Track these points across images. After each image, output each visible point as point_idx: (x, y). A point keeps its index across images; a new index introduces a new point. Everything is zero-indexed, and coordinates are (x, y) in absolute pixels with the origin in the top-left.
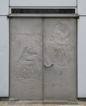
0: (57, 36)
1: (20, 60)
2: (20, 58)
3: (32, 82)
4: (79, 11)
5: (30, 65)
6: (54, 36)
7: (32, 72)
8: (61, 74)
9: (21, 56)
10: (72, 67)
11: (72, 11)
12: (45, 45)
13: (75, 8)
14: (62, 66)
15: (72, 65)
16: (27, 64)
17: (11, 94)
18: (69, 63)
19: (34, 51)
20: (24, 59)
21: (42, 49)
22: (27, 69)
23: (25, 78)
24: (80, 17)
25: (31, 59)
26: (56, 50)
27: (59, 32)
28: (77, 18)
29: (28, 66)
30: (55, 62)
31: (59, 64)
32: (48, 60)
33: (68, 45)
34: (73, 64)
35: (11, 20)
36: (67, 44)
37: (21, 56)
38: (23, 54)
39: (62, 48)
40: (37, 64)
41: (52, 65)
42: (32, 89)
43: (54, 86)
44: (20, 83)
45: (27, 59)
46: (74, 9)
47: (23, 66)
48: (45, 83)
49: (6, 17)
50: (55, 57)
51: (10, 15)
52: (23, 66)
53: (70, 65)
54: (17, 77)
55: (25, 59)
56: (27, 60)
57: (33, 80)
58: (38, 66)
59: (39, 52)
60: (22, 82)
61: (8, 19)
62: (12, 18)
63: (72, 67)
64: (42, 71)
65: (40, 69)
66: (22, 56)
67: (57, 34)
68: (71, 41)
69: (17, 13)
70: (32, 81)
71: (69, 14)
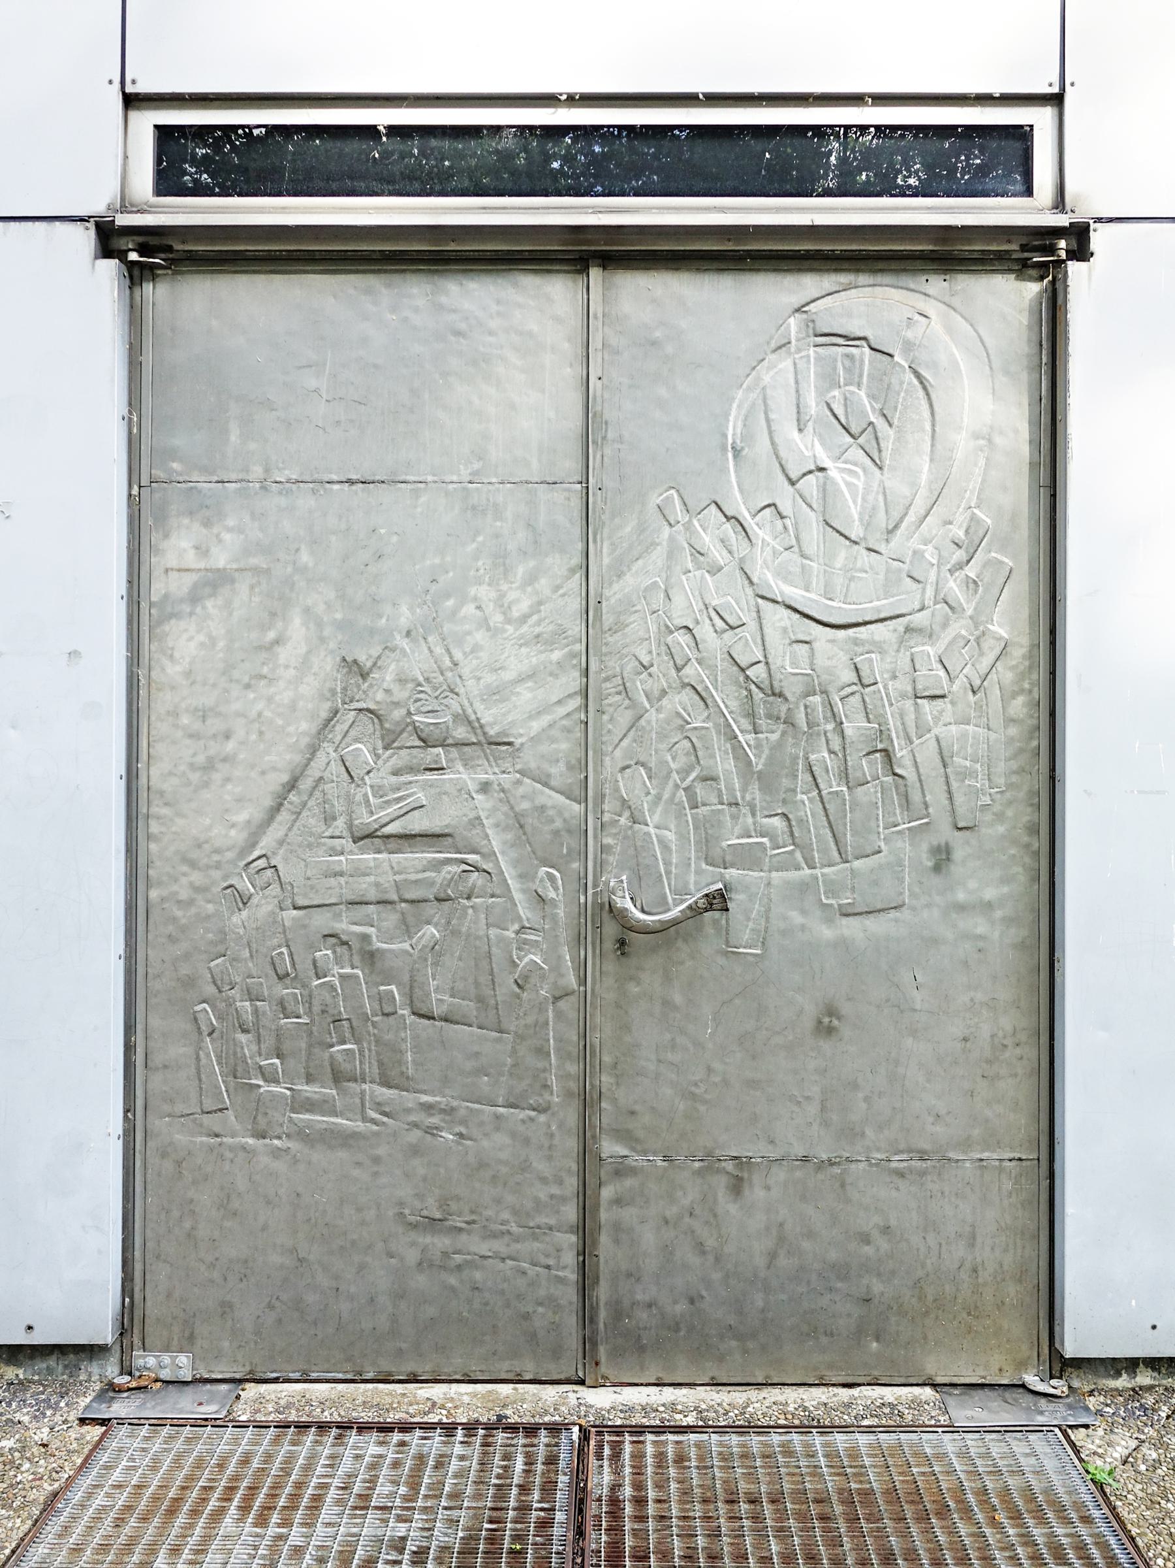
0: (786, 507)
1: (266, 843)
2: (277, 808)
3: (431, 1131)
4: (1090, 166)
5: (409, 906)
6: (738, 505)
7: (439, 1000)
8: (827, 1025)
9: (292, 785)
10: (980, 926)
11: (1000, 154)
12: (618, 627)
13: (1040, 119)
14: (846, 913)
15: (988, 907)
16: (365, 887)
17: (154, 1307)
18: (937, 869)
19: (462, 718)
20: (329, 819)
21: (572, 680)
22: (371, 957)
23: (338, 1077)
24: (1099, 239)
25: (417, 823)
26: (765, 696)
27: (807, 447)
28: (1048, 253)
29: (390, 919)
30: (748, 858)
31: (805, 887)
32: (660, 829)
33: (929, 635)
34: (990, 894)
35: (154, 292)
36: (920, 619)
37: (285, 778)
38: (313, 750)
39: (848, 676)
40: (507, 892)
41: (718, 901)
42: (432, 1224)
43: (737, 1187)
44: (276, 1153)
45: (365, 819)
46: (1022, 135)
47: (321, 921)
48: (610, 1148)
49: (85, 239)
50: (755, 793)
51: (125, 206)
52: (321, 921)
53: (961, 908)
54: (235, 1069)
55: (340, 824)
56: (366, 837)
57: (450, 1111)
58: (525, 912)
59: (536, 726)
60: (302, 1134)
61: (110, 267)
62: (154, 241)
63: (980, 926)
64: (572, 981)
65: (550, 959)
66: (305, 784)
67: (640, 1446)
68: (971, 571)
69: (238, 193)
70: (435, 1120)
71: (945, 196)
